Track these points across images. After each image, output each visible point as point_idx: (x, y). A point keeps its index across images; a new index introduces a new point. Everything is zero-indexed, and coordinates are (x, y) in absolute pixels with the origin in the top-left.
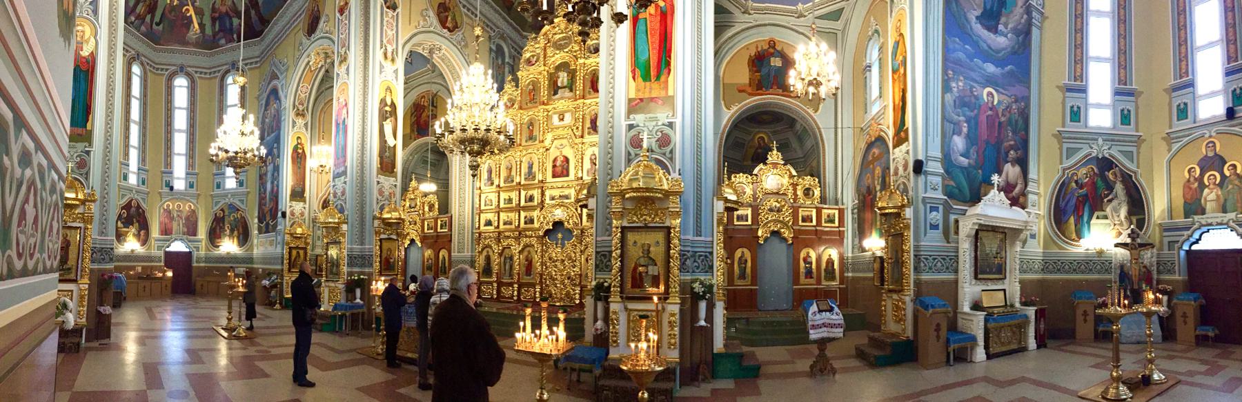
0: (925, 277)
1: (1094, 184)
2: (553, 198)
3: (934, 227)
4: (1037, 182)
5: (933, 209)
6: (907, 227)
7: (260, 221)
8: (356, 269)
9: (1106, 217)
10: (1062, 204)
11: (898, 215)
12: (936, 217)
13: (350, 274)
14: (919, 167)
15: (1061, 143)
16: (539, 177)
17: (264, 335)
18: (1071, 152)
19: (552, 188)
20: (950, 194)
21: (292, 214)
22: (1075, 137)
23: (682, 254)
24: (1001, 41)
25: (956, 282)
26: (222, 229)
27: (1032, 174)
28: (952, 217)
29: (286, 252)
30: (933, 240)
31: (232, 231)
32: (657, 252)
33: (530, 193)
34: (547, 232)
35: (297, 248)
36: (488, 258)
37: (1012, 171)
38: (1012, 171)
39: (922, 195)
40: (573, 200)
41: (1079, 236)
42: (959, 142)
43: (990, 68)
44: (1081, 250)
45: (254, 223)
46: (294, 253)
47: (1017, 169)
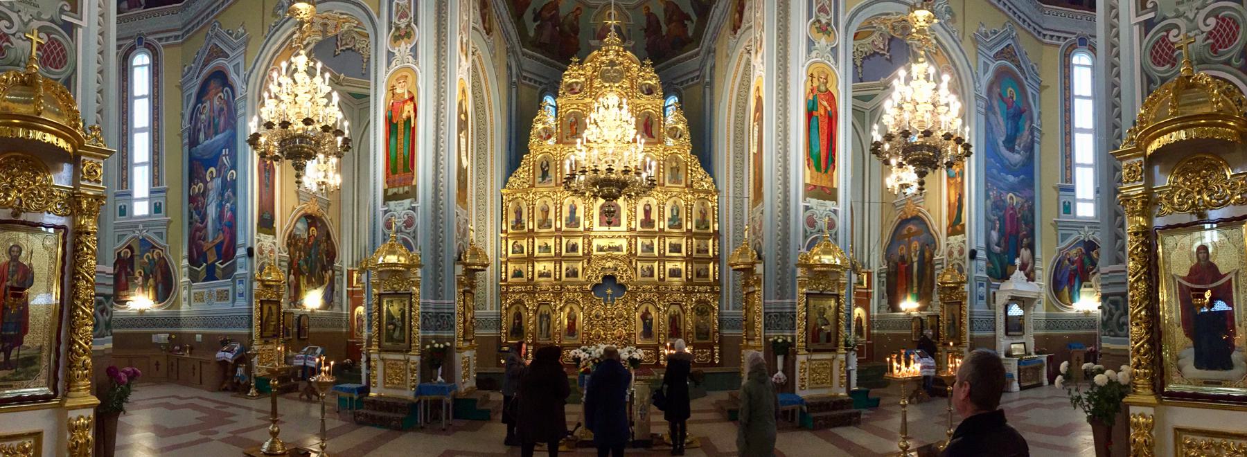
0: (976, 334)
1: (1082, 261)
2: (601, 249)
3: (981, 298)
4: (1041, 260)
5: (981, 285)
6: (965, 298)
7: (192, 261)
8: (431, 334)
9: (1091, 286)
10: (1059, 277)
11: (955, 288)
12: (982, 290)
13: (425, 340)
14: (973, 255)
15: (1056, 230)
16: (583, 224)
17: (191, 429)
18: (1064, 237)
19: (601, 237)
20: (989, 273)
21: (261, 252)
22: (1066, 225)
23: (425, 316)
24: (1016, 158)
25: (995, 337)
26: (130, 276)
27: (1038, 255)
28: (992, 291)
29: (255, 305)
30: (981, 308)
31: (146, 278)
32: (830, 314)
33: (573, 241)
34: (596, 287)
35: (269, 301)
36: (518, 316)
37: (1025, 253)
38: (1025, 253)
39: (974, 275)
40: (625, 252)
41: (1072, 301)
42: (995, 235)
43: (1011, 178)
44: (1074, 312)
45: (181, 267)
46: (266, 307)
47: (1029, 251)
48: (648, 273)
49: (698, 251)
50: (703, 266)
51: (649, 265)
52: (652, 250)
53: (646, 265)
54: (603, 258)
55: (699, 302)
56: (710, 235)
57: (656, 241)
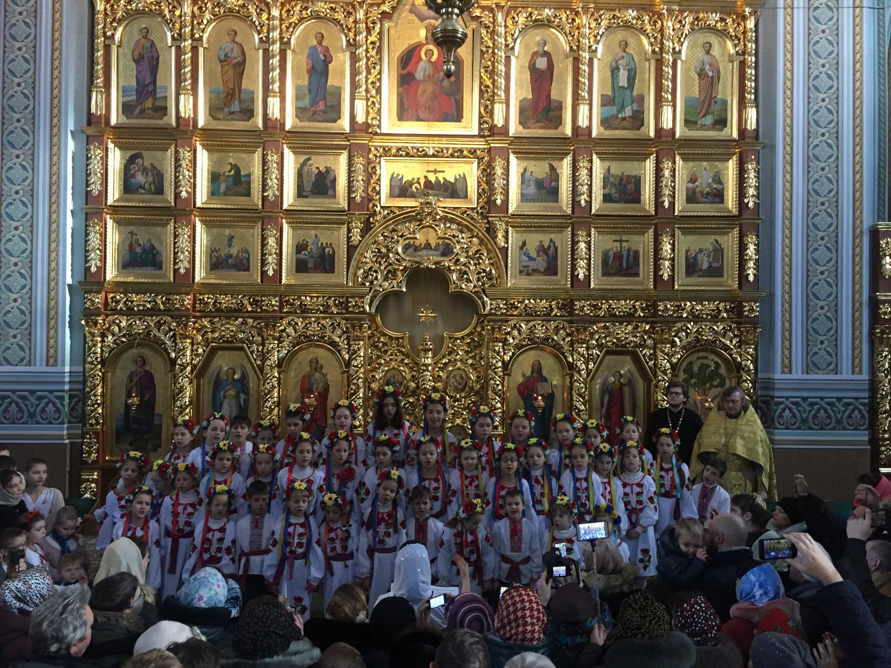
2: (402, 189)
16: (353, 110)
19: (403, 153)
33: (319, 162)
34: (388, 301)
36: (144, 383)
48: (541, 263)
49: (692, 198)
50: (707, 242)
51: (545, 238)
52: (554, 193)
53: (534, 240)
54: (416, 217)
55: (696, 346)
56: (728, 143)
57: (565, 168)
